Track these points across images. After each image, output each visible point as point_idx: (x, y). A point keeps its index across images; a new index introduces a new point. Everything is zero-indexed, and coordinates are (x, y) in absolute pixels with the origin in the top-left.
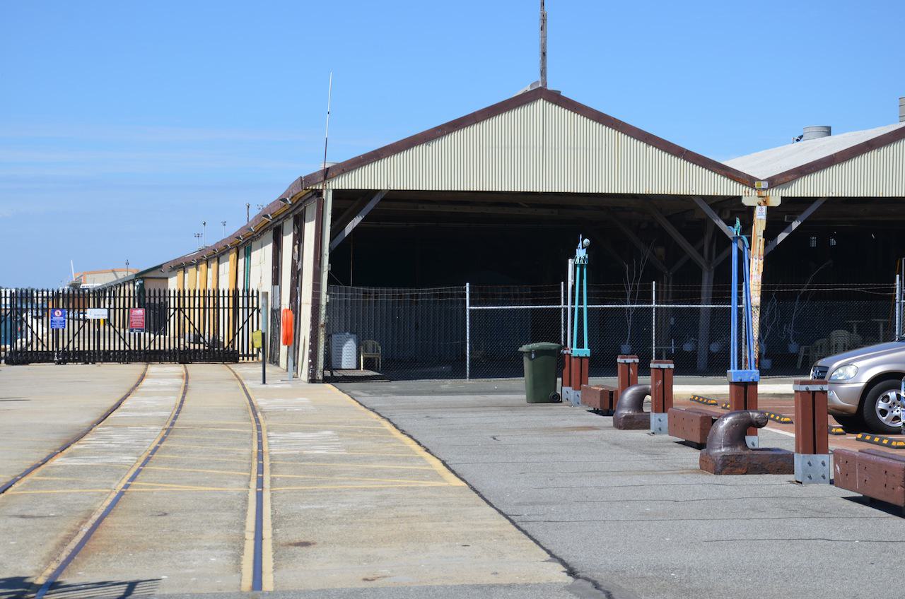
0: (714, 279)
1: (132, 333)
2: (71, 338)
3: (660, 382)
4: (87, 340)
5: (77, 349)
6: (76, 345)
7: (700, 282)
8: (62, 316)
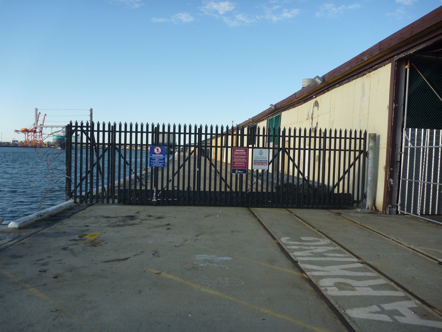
0: (315, 240)
1: (234, 174)
2: (171, 178)
3: (325, 91)
4: (208, 176)
5: (176, 188)
6: (176, 184)
7: (415, 141)
8: (161, 154)
